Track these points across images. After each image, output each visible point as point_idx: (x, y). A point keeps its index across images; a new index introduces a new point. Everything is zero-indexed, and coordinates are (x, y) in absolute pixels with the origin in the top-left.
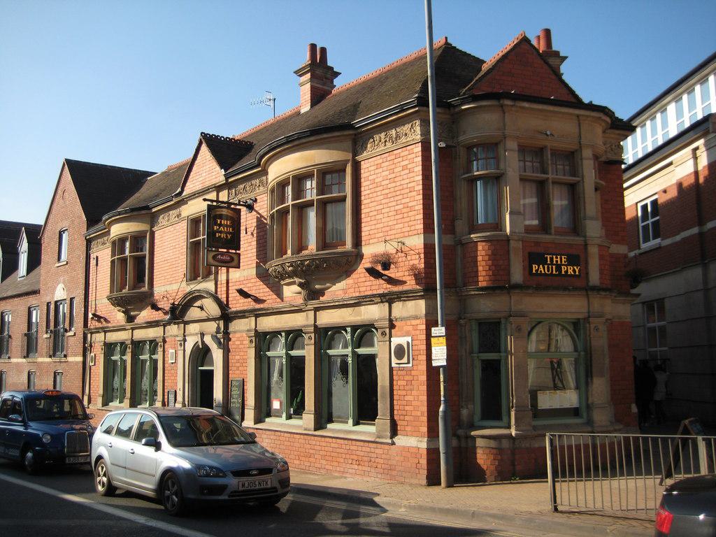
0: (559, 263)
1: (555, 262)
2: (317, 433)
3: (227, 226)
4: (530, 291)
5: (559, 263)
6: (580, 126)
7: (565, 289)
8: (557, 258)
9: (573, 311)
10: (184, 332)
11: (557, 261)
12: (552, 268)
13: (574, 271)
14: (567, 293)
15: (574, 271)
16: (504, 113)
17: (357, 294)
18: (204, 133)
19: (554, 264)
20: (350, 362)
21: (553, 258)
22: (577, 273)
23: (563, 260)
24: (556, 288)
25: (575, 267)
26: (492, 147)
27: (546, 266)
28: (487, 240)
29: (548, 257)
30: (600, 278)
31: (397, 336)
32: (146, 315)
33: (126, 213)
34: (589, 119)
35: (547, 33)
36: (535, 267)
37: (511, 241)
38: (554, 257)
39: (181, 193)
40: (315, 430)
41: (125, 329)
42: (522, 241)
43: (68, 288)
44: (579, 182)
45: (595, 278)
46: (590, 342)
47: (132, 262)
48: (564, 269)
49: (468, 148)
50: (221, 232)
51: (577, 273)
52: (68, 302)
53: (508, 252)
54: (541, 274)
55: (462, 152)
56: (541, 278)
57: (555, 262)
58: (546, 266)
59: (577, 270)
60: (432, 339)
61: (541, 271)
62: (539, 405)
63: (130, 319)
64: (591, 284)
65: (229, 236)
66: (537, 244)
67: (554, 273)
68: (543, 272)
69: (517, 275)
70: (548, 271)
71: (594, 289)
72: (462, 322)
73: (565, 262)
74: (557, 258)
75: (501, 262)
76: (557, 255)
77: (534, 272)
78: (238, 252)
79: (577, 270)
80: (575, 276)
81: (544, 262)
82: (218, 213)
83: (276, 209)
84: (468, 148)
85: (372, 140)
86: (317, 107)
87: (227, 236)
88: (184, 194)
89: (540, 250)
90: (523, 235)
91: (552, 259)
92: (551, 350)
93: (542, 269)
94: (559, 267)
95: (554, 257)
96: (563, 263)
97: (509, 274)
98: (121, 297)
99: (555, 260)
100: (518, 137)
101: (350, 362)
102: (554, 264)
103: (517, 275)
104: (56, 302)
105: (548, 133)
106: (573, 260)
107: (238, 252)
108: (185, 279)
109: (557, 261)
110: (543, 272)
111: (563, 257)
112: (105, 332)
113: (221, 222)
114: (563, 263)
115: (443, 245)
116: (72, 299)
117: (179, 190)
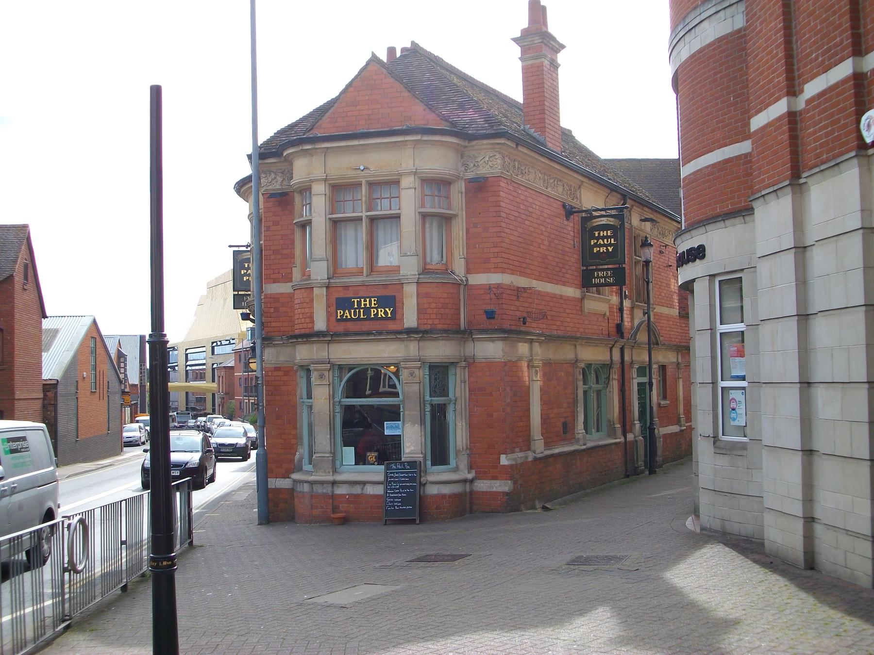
0: (368, 306)
3: (607, 237)
11: (365, 305)
12: (359, 312)
13: (386, 313)
15: (386, 313)
21: (361, 301)
25: (387, 309)
27: (352, 311)
29: (356, 300)
30: (418, 319)
34: (408, 143)
36: (340, 313)
38: (362, 300)
45: (410, 319)
46: (421, 429)
48: (373, 312)
50: (600, 246)
51: (389, 316)
53: (312, 300)
54: (347, 320)
57: (363, 306)
58: (352, 311)
59: (389, 312)
61: (346, 316)
65: (610, 249)
67: (362, 317)
68: (349, 317)
70: (355, 315)
71: (410, 332)
73: (375, 304)
76: (360, 298)
78: (236, 293)
79: (389, 312)
80: (386, 319)
86: (249, 202)
87: (607, 249)
89: (350, 294)
90: (325, 281)
91: (359, 303)
92: (125, 501)
93: (348, 315)
94: (367, 311)
95: (362, 300)
96: (373, 306)
97: (313, 322)
107: (236, 293)
109: (365, 305)
110: (349, 317)
111: (373, 299)
113: (599, 234)
114: (373, 306)
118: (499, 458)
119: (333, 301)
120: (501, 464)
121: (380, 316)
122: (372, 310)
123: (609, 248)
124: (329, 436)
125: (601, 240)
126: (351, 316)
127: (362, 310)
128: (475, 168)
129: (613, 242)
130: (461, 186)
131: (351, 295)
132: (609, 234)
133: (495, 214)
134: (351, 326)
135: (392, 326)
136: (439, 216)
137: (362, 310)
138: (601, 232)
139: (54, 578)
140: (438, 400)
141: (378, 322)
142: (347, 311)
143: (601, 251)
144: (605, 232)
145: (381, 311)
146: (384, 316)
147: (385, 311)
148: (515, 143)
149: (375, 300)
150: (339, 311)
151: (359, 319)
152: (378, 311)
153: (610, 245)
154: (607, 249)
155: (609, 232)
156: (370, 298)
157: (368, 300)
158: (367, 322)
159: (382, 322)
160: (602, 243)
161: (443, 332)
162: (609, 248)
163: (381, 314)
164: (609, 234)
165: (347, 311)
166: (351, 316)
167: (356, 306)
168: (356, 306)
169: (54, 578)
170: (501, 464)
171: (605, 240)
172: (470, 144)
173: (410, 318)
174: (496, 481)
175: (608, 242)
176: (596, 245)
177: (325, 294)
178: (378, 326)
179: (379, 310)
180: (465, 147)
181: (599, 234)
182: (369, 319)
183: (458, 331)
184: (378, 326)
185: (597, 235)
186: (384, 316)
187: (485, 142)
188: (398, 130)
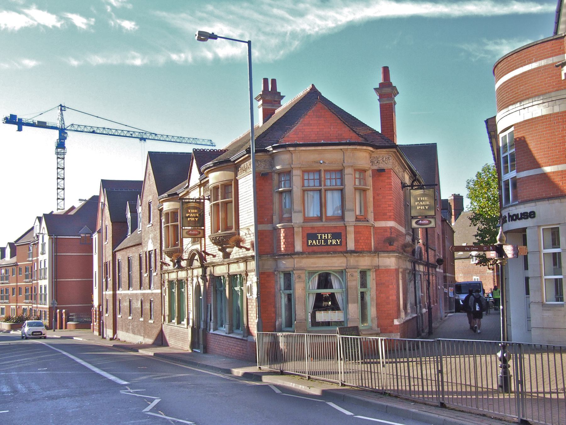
0: (326, 238)
1: (323, 238)
2: (231, 335)
3: (195, 213)
4: (305, 256)
5: (326, 238)
6: (121, 222)
7: (328, 253)
8: (325, 235)
9: (337, 265)
10: (193, 275)
11: (325, 237)
12: (322, 241)
13: (337, 242)
14: (330, 255)
15: (337, 242)
16: (292, 154)
17: (238, 257)
18: (195, 149)
19: (323, 239)
20: (240, 295)
21: (322, 235)
22: (339, 243)
23: (329, 236)
24: (322, 253)
25: (337, 240)
26: (288, 173)
27: (317, 241)
28: (283, 227)
29: (319, 235)
31: (159, 294)
32: (236, 253)
33: (166, 197)
34: (348, 150)
35: (80, 200)
37: (295, 228)
38: (323, 235)
39: (188, 186)
40: (229, 334)
41: (223, 264)
42: (302, 227)
43: (154, 245)
44: (343, 188)
47: (172, 229)
48: (329, 242)
49: (279, 174)
51: (339, 243)
52: (153, 252)
54: (314, 245)
55: (276, 177)
56: (315, 247)
57: (323, 238)
58: (317, 241)
59: (339, 242)
60: (456, 261)
61: (314, 244)
62: (316, 319)
63: (227, 255)
64: (348, 249)
65: (197, 219)
66: (313, 228)
67: (323, 244)
68: (315, 244)
69: (298, 247)
70: (319, 243)
71: (352, 252)
72: (276, 273)
73: (330, 237)
74: (325, 235)
75: (289, 240)
76: (322, 234)
77: (309, 244)
79: (339, 242)
80: (337, 245)
81: (316, 238)
82: (189, 206)
83: (213, 203)
84: (279, 174)
85: (240, 169)
87: (195, 219)
88: (190, 187)
90: (302, 224)
91: (321, 236)
93: (315, 243)
94: (326, 241)
95: (323, 235)
96: (329, 238)
98: (168, 251)
99: (323, 236)
100: (300, 168)
101: (240, 295)
102: (323, 239)
103: (298, 247)
104: (149, 252)
105: (321, 162)
106: (336, 236)
108: (191, 242)
109: (325, 237)
111: (329, 235)
112: (168, 273)
113: (191, 211)
115: (258, 231)
116: (155, 250)
117: (187, 184)
118: (393, 321)
119: (305, 235)
120: (394, 324)
121: (333, 244)
122: (329, 240)
123: (426, 207)
124: (304, 310)
125: (421, 202)
126: (316, 243)
127: (323, 241)
128: (377, 164)
129: (198, 216)
130: (370, 173)
131: (316, 232)
132: (196, 212)
133: (389, 189)
134: (315, 248)
135: (339, 249)
136: (359, 189)
137: (323, 241)
138: (192, 210)
139: (439, 364)
140: (363, 290)
141: (332, 247)
142: (314, 241)
143: (422, 208)
144: (424, 198)
145: (334, 241)
146: (335, 244)
147: (336, 241)
148: (368, 153)
149: (330, 235)
150: (309, 241)
151: (321, 245)
152: (332, 241)
153: (196, 217)
154: (195, 219)
155: (426, 198)
156: (328, 234)
157: (326, 235)
158: (326, 247)
159: (334, 247)
160: (422, 204)
161: (366, 252)
162: (426, 207)
163: (334, 242)
164: (196, 212)
165: (314, 241)
166: (316, 243)
167: (319, 238)
168: (319, 238)
169: (439, 364)
170: (394, 324)
171: (194, 214)
172: (376, 151)
173: (351, 245)
174: (391, 334)
175: (425, 203)
176: (189, 217)
177: (301, 231)
178: (332, 248)
179: (333, 240)
180: (373, 152)
181: (191, 211)
182: (327, 245)
183: (370, 251)
184: (332, 248)
185: (189, 211)
186: (335, 244)
187: (384, 150)
188: (329, 143)
